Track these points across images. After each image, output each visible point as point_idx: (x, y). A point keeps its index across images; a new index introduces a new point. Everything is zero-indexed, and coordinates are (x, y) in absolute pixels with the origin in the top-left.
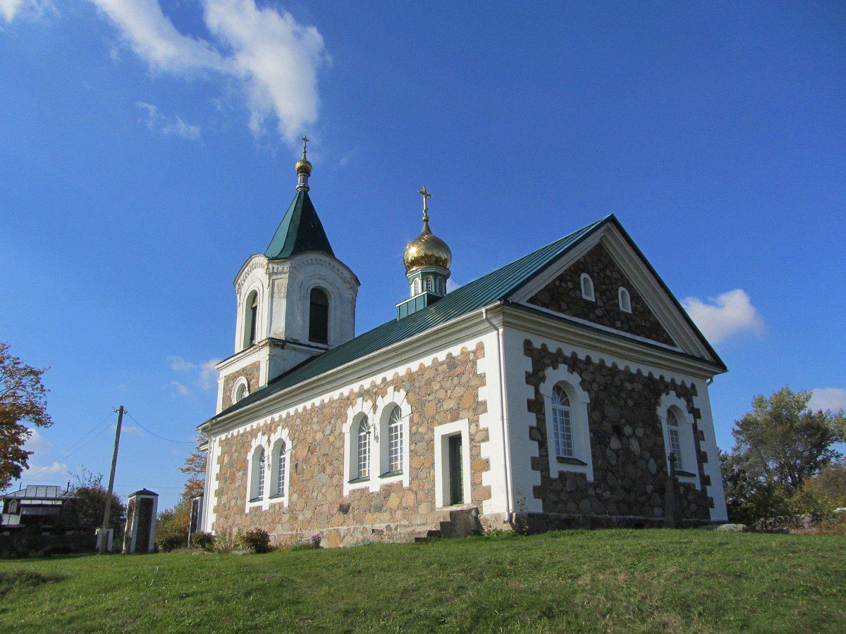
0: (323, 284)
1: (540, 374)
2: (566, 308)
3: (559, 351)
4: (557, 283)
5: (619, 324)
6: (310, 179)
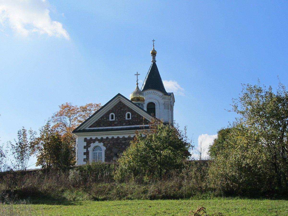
0: (151, 101)
1: (89, 145)
2: (103, 125)
3: (91, 138)
4: (100, 119)
5: (124, 124)
6: (156, 57)
